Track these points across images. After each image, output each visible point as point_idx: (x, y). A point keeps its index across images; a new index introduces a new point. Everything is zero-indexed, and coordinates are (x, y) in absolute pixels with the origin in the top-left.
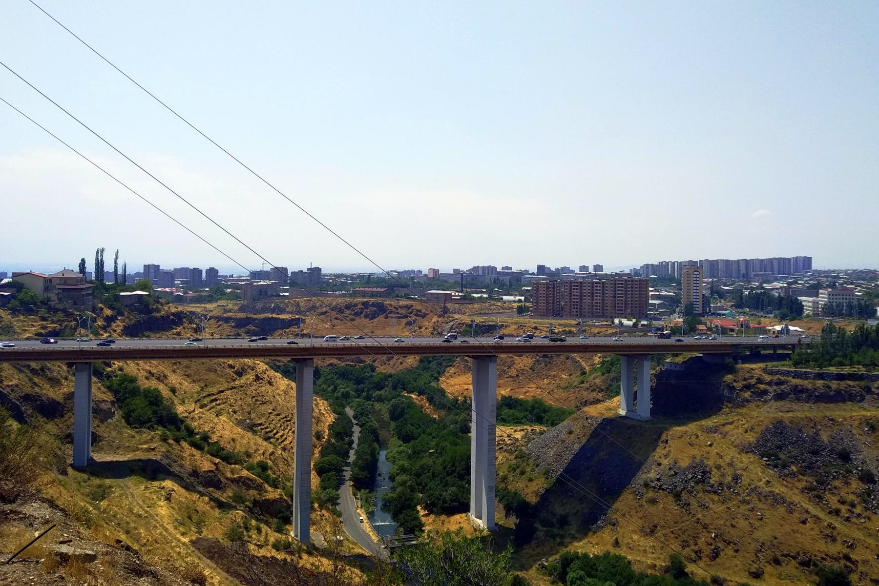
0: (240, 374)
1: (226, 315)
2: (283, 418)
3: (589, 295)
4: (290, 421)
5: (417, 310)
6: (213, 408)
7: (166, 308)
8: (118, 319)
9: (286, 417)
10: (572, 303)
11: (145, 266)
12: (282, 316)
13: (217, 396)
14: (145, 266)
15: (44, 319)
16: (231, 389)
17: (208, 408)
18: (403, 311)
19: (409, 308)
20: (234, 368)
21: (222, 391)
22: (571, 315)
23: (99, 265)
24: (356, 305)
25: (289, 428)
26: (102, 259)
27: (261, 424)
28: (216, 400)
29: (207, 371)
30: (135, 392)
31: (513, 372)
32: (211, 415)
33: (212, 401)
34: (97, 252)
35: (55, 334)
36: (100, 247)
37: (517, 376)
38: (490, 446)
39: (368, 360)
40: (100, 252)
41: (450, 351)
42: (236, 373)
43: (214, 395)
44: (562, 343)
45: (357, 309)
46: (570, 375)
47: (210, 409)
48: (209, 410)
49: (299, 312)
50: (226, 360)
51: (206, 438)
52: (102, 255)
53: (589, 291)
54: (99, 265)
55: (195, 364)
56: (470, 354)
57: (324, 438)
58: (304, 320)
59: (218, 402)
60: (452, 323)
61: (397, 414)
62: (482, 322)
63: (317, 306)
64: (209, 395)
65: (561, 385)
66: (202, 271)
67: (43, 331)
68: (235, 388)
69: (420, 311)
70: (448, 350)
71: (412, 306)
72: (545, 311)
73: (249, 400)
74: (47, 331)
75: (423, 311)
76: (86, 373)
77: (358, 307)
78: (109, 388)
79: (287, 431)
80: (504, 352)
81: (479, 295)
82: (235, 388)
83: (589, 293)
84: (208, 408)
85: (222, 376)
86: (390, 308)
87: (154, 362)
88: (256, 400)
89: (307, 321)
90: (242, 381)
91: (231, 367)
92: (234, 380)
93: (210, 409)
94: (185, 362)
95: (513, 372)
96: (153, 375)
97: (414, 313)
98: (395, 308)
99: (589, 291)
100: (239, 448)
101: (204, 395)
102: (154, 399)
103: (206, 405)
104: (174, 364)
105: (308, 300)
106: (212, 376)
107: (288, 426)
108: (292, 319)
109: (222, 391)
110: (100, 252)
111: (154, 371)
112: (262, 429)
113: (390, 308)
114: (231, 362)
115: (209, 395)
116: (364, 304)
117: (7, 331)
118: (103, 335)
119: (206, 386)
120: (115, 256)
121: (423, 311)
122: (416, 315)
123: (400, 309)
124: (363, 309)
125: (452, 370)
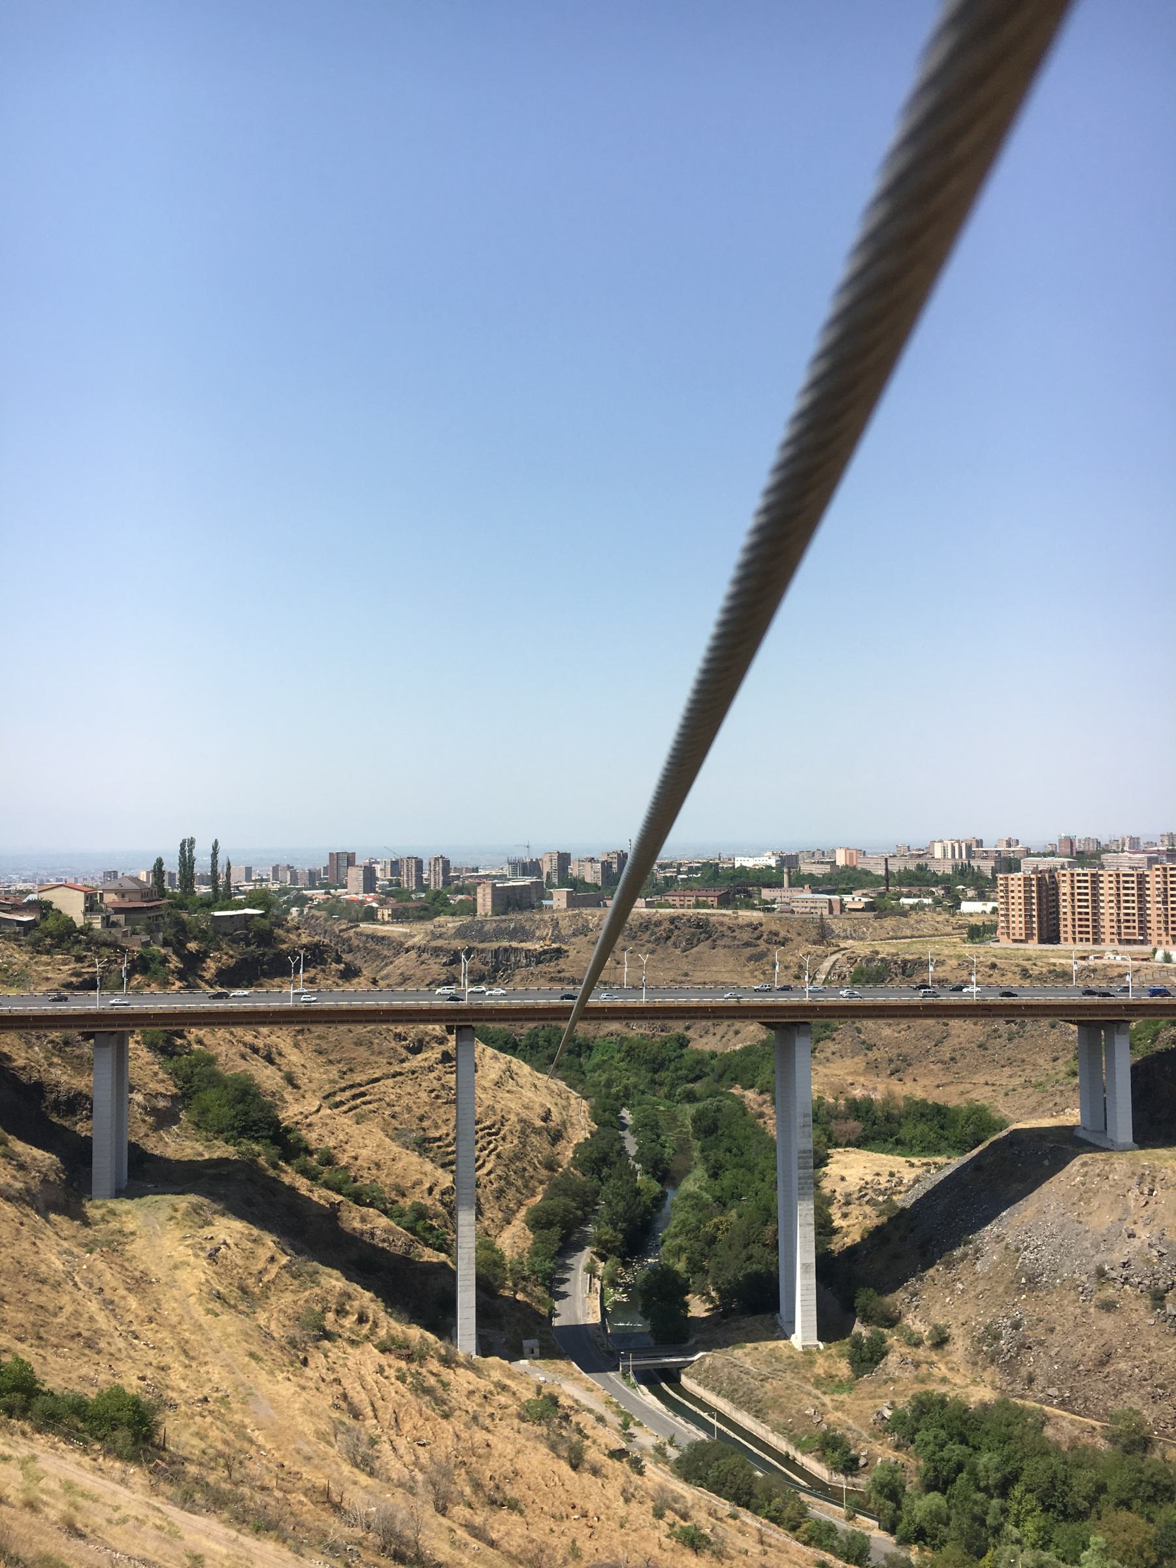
0: (416, 1050)
1: (434, 944)
2: (482, 1130)
3: (1112, 898)
4: (496, 1134)
5: (771, 932)
6: (355, 1108)
7: (293, 937)
8: (210, 957)
9: (489, 1128)
10: (1077, 917)
11: (331, 854)
12: (528, 945)
13: (368, 1087)
14: (331, 854)
15: (79, 959)
16: (394, 1076)
17: (345, 1108)
18: (746, 936)
19: (756, 929)
20: (405, 1039)
21: (377, 1080)
22: (1074, 939)
23: (187, 863)
24: (658, 924)
25: (492, 1146)
26: (191, 855)
27: (440, 1139)
28: (363, 1094)
29: (356, 1044)
30: (215, 1080)
31: (946, 1051)
32: (345, 1121)
33: (354, 1097)
34: (183, 845)
35: (89, 985)
36: (187, 837)
37: (952, 1059)
38: (803, 1188)
39: (677, 1027)
40: (187, 847)
41: (717, 1015)
42: (407, 1048)
43: (360, 1085)
44: (1107, 1000)
45: (661, 931)
46: (1055, 1059)
47: (350, 1110)
48: (346, 1112)
49: (557, 937)
50: (392, 1027)
51: (328, 1160)
52: (191, 851)
53: (1111, 892)
54: (187, 863)
55: (336, 1032)
56: (1073, 1019)
57: (561, 1167)
58: (567, 951)
59: (368, 1098)
60: (834, 958)
61: (708, 1127)
62: (893, 955)
63: (591, 926)
64: (352, 1087)
65: (1033, 1080)
66: (422, 861)
67: (74, 979)
68: (401, 1074)
69: (777, 934)
70: (990, 1010)
71: (761, 925)
72: (1023, 931)
73: (424, 1096)
74: (81, 979)
75: (783, 934)
76: (109, 1049)
77: (663, 928)
78: (174, 1073)
79: (487, 1152)
80: (55, 1027)
81: (916, 900)
82: (401, 1074)
83: (1111, 895)
84: (345, 1108)
85: (380, 1053)
86: (720, 928)
87: (264, 1030)
88: (437, 1097)
89: (572, 954)
90: (416, 1061)
91: (399, 1037)
92: (403, 1061)
93: (350, 1110)
94: (319, 1029)
95: (946, 1051)
96: (255, 1050)
97: (765, 937)
98: (730, 928)
99: (1111, 892)
100: (385, 1180)
101: (343, 1085)
102: (246, 1092)
103: (342, 1103)
104: (299, 1031)
105: (574, 916)
106: (362, 1053)
107: (490, 1143)
108: (544, 951)
109: (377, 1080)
110: (187, 847)
111: (260, 1043)
112: (439, 1147)
113: (720, 928)
114: (400, 1029)
115: (352, 1087)
116: (672, 920)
117: (18, 979)
118: (174, 984)
119: (351, 1070)
120: (211, 851)
121: (783, 934)
122: (768, 942)
123: (737, 930)
124: (671, 931)
125: (831, 1047)
